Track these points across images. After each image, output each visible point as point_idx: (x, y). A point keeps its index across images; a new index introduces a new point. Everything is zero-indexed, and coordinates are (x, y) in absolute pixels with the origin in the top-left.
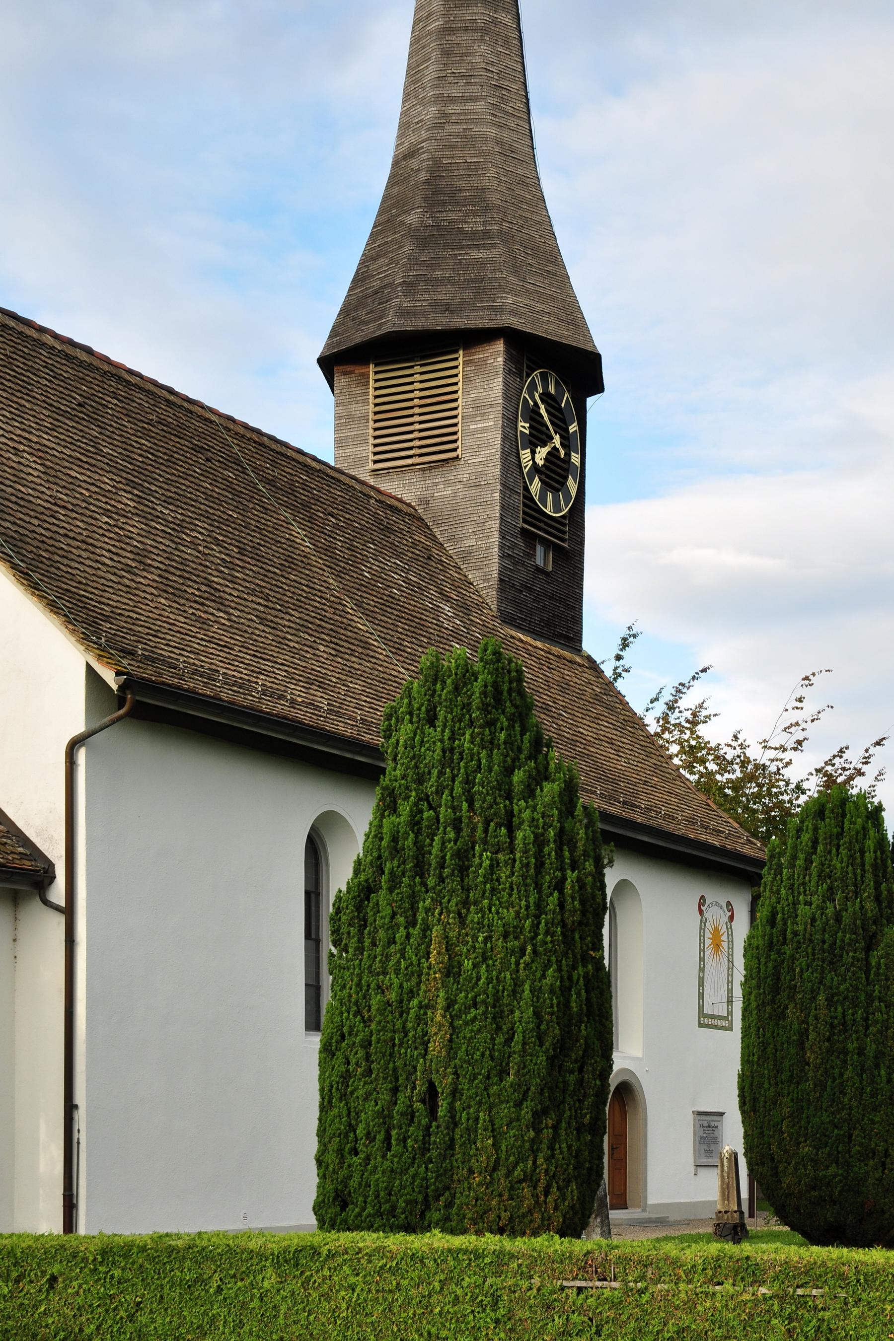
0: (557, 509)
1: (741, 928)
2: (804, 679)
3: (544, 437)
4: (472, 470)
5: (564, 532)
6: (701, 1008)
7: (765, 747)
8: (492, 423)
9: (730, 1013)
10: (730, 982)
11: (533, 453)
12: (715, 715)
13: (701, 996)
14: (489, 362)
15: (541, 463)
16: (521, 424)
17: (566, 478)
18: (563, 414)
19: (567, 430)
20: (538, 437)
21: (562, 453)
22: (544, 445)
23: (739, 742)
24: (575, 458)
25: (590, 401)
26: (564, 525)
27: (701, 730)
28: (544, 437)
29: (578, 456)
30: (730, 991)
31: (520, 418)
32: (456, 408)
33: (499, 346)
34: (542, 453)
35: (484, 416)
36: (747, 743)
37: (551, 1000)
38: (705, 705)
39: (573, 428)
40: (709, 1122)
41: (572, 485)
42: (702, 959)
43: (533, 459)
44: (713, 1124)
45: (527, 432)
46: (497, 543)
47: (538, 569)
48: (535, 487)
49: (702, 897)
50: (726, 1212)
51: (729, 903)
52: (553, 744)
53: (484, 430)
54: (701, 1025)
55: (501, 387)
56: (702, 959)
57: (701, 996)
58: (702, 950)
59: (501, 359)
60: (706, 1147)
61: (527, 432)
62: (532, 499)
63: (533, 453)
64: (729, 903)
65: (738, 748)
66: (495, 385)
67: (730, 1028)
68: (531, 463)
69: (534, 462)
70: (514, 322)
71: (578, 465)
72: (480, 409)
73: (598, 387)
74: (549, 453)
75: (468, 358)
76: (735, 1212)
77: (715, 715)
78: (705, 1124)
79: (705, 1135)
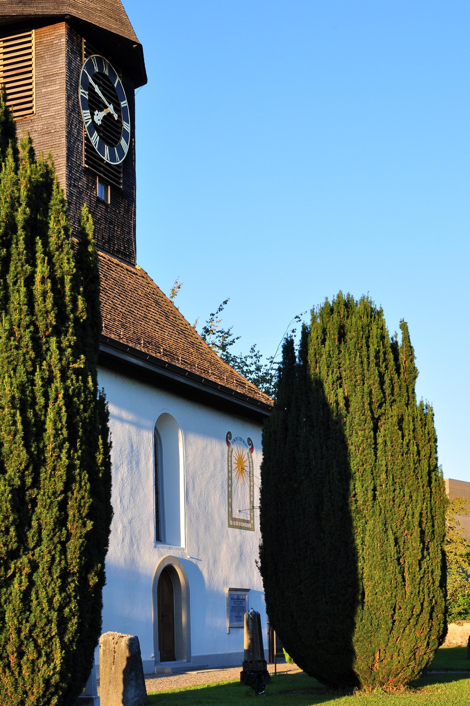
0: (113, 158)
1: (258, 458)
2: (295, 318)
3: (102, 106)
4: (44, 122)
5: (119, 178)
6: (230, 513)
7: (271, 362)
8: (59, 87)
9: (252, 518)
10: (252, 496)
11: (92, 115)
12: (237, 338)
13: (230, 505)
14: (55, 42)
15: (99, 123)
16: (81, 90)
17: (119, 139)
18: (115, 93)
19: (119, 105)
20: (94, 104)
21: (116, 116)
22: (101, 110)
23: (255, 353)
24: (126, 126)
25: (138, 91)
26: (119, 173)
27: (231, 350)
28: (102, 106)
29: (129, 125)
30: (252, 502)
31: (80, 86)
32: (31, 78)
33: (61, 29)
34: (99, 117)
35: (53, 82)
36: (260, 354)
37: (14, 415)
38: (230, 333)
39: (124, 104)
40: (238, 596)
41: (124, 144)
42: (230, 478)
43: (92, 118)
44: (241, 597)
45: (87, 97)
46: (65, 175)
47: (99, 200)
48: (95, 139)
49: (229, 433)
50: (251, 662)
51: (249, 439)
52: (11, 109)
53: (52, 93)
54: (230, 526)
55: (64, 60)
56: (230, 478)
57: (230, 505)
58: (230, 472)
59: (64, 40)
60: (236, 614)
61: (87, 97)
62: (93, 149)
63: (92, 115)
64: (249, 439)
65: (254, 357)
66: (60, 59)
67: (252, 529)
68: (91, 121)
69: (93, 121)
70: (74, 12)
71: (129, 130)
72: (48, 78)
73: (142, 79)
74: (104, 117)
75: (39, 41)
76: (259, 661)
77: (237, 338)
78: (235, 597)
79: (235, 605)
